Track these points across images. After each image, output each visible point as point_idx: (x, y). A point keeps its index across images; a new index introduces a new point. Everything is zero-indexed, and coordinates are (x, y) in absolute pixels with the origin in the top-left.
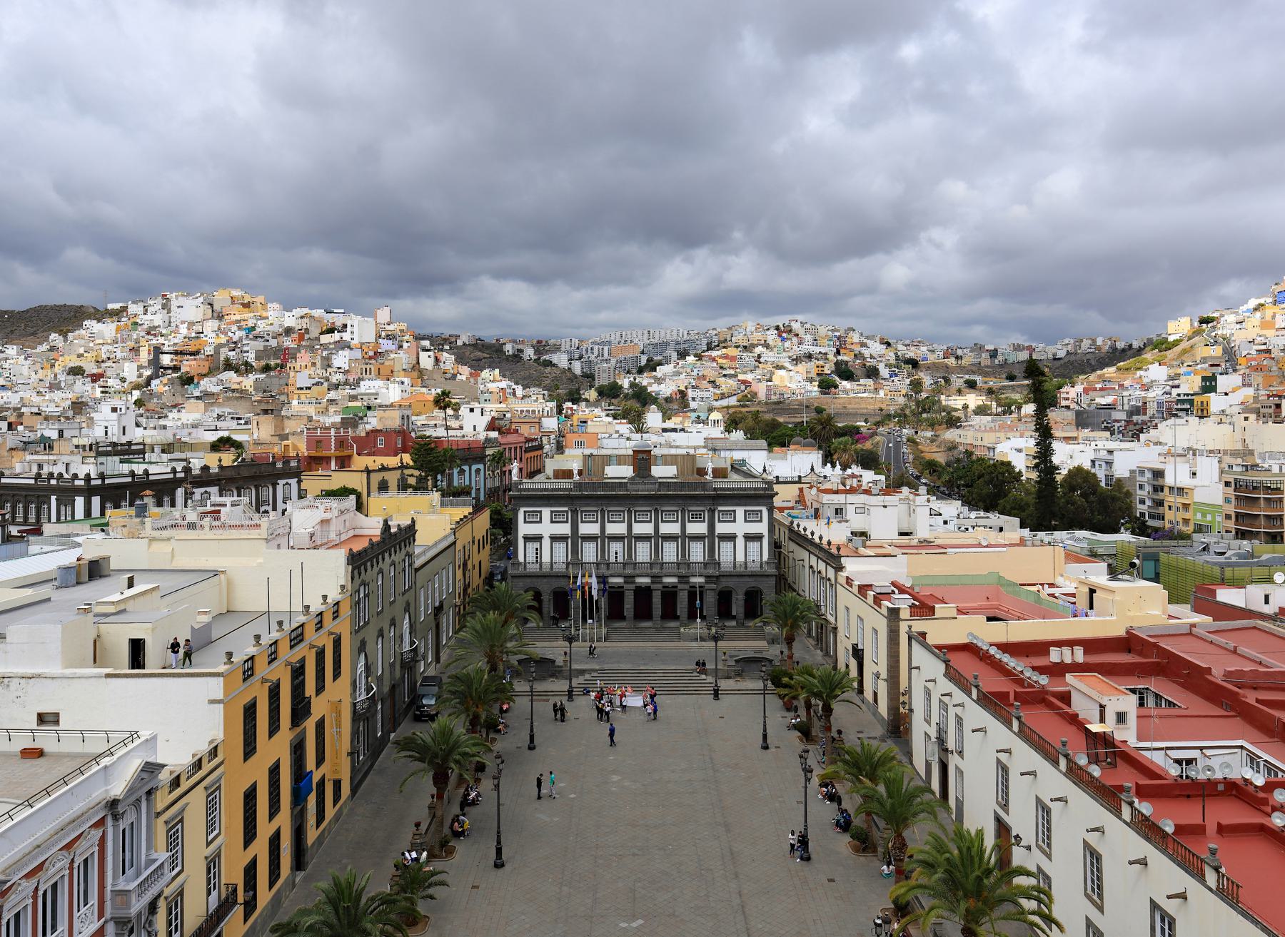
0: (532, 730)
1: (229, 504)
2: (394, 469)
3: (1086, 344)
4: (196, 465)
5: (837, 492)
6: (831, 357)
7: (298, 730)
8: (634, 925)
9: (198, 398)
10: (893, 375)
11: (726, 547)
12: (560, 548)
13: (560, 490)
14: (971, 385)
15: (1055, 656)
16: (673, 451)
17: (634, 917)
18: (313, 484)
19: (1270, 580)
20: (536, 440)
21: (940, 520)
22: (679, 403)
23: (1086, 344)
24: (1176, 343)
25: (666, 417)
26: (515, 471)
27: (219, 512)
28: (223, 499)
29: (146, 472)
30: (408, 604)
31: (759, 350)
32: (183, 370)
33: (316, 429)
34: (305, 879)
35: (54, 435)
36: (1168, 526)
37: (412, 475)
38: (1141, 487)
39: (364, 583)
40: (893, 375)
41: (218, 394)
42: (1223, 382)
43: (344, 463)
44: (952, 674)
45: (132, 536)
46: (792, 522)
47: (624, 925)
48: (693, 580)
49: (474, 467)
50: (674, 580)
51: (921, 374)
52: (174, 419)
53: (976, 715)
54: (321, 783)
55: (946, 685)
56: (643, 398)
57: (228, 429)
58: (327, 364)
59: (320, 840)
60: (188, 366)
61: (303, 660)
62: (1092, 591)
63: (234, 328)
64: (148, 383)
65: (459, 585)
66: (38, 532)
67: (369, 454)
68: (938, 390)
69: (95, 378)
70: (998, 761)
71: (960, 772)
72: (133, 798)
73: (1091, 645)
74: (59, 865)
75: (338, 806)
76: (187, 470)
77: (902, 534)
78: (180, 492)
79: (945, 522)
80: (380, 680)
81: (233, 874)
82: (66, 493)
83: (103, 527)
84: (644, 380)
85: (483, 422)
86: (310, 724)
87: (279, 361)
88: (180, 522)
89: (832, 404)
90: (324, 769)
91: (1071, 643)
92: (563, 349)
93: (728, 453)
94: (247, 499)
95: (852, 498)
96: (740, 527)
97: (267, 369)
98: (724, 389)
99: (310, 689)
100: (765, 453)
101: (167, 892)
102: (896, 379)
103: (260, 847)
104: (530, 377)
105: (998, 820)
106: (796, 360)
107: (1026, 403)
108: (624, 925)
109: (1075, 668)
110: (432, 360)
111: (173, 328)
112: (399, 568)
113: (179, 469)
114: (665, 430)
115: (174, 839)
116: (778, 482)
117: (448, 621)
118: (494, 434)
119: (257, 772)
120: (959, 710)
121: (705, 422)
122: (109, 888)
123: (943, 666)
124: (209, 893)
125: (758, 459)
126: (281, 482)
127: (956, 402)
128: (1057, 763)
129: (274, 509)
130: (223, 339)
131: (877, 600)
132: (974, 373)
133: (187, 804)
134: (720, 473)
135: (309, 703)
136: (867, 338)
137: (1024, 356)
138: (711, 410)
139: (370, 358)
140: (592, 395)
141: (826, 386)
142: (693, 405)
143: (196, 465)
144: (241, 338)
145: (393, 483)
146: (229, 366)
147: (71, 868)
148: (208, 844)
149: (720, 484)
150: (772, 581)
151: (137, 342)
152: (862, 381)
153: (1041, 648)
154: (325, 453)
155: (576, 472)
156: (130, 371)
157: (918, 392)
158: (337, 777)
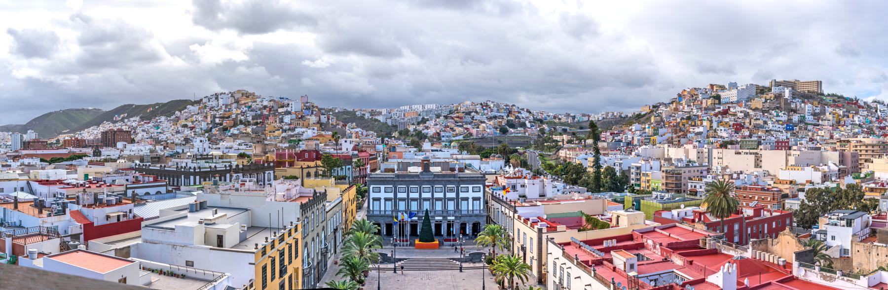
3: (610, 116)
4: (234, 164)
10: (532, 126)
11: (464, 203)
12: (389, 203)
14: (565, 131)
15: (605, 244)
16: (438, 160)
18: (280, 171)
19: (679, 207)
22: (437, 138)
23: (610, 116)
24: (645, 115)
31: (473, 114)
35: (181, 151)
39: (307, 217)
40: (532, 126)
42: (661, 131)
43: (291, 165)
44: (565, 254)
45: (212, 192)
50: (441, 218)
52: (223, 144)
53: (576, 271)
55: (563, 260)
56: (421, 136)
57: (243, 149)
58: (281, 121)
62: (618, 217)
65: (344, 219)
66: (179, 189)
68: (551, 133)
69: (192, 128)
73: (620, 239)
76: (231, 166)
78: (228, 175)
80: (313, 260)
82: (187, 174)
83: (202, 189)
84: (420, 128)
86: (286, 277)
89: (506, 139)
91: (611, 238)
95: (519, 181)
96: (470, 195)
97: (257, 124)
98: (457, 132)
99: (286, 262)
106: (490, 119)
117: (339, 235)
118: (356, 152)
120: (569, 270)
121: (449, 147)
125: (476, 163)
127: (558, 138)
130: (239, 112)
134: (461, 170)
137: (586, 119)
138: (451, 142)
140: (396, 134)
141: (504, 131)
142: (443, 139)
143: (234, 164)
145: (313, 174)
146: (241, 122)
149: (461, 175)
150: (485, 219)
153: (599, 242)
156: (204, 125)
157: (544, 133)
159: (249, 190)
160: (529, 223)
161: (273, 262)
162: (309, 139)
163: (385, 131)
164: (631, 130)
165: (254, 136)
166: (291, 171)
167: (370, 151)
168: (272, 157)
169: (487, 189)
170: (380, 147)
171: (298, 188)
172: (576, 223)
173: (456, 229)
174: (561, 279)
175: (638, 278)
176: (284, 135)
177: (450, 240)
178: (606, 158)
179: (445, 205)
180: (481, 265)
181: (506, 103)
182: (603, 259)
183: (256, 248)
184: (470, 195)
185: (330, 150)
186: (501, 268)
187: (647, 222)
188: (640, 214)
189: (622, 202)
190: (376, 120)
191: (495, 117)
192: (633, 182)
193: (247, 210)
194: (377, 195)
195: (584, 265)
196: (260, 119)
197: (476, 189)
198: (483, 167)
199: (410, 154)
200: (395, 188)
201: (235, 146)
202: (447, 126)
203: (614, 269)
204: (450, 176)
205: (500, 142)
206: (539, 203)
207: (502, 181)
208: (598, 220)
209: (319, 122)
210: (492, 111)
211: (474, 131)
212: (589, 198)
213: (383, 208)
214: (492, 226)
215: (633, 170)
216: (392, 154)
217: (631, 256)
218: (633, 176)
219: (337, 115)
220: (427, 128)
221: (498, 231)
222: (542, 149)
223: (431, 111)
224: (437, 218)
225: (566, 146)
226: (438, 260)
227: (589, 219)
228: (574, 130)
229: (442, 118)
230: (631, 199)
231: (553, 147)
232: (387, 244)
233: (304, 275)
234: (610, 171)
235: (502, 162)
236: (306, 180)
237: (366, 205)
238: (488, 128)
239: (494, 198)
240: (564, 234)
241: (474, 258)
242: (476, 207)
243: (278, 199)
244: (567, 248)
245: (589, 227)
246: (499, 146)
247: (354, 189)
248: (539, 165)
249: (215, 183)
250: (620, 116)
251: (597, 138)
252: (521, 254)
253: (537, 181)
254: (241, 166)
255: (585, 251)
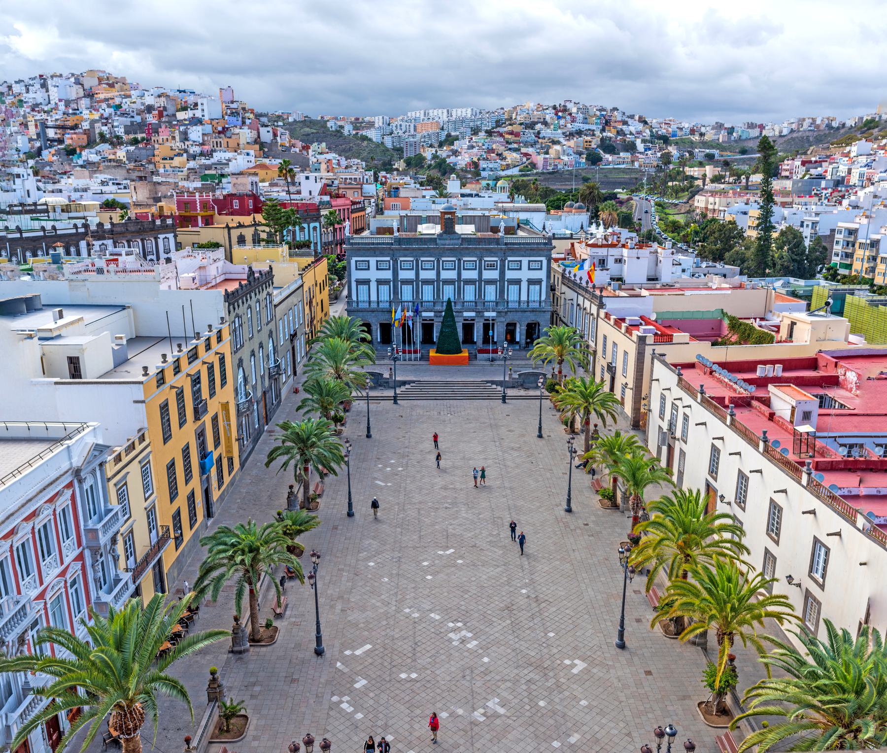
0: (368, 424)
1: (123, 253)
2: (249, 226)
3: (806, 125)
5: (602, 246)
6: (598, 133)
7: (199, 423)
8: (448, 552)
9: (82, 166)
10: (647, 149)
11: (513, 288)
12: (384, 289)
13: (383, 244)
14: (710, 158)
15: (760, 372)
16: (471, 213)
17: (447, 548)
18: (186, 235)
20: (360, 203)
21: (679, 268)
22: (474, 171)
23: (806, 125)
25: (463, 185)
26: (347, 229)
27: (117, 260)
28: (117, 250)
29: (54, 228)
30: (271, 332)
31: (539, 127)
32: (68, 142)
33: (182, 192)
34: (214, 523)
36: (853, 273)
37: (264, 231)
38: (837, 242)
39: (238, 316)
40: (647, 149)
41: (99, 163)
43: (208, 221)
46: (564, 270)
47: (441, 552)
48: (487, 314)
49: (312, 225)
50: (473, 314)
51: (670, 149)
52: (66, 183)
53: (699, 413)
54: (220, 459)
56: (444, 169)
58: (185, 137)
59: (221, 498)
60: (70, 139)
61: (199, 372)
62: (793, 324)
63: (104, 105)
64: (39, 152)
67: (226, 214)
68: (683, 163)
70: (713, 445)
71: (682, 453)
72: (90, 468)
73: (789, 365)
74: (46, 513)
75: (232, 475)
76: (86, 226)
77: (649, 280)
78: (83, 244)
79: (684, 271)
80: (254, 388)
81: (164, 519)
84: (443, 153)
85: (317, 187)
86: (207, 419)
87: (144, 135)
88: (90, 267)
90: (222, 449)
91: (773, 362)
92: (376, 125)
93: (515, 214)
94: (136, 250)
95: (612, 251)
97: (135, 142)
98: (509, 161)
99: (205, 394)
100: (544, 214)
101: (122, 530)
102: (649, 152)
103: (181, 502)
104: (350, 149)
105: (708, 485)
106: (570, 135)
107: (754, 173)
108: (441, 552)
109: (776, 380)
110: (271, 134)
111: (52, 105)
112: (263, 304)
113: (79, 225)
114: (463, 195)
115: (123, 496)
116: (555, 239)
117: (300, 344)
118: (326, 198)
119: (174, 450)
120: (687, 411)
121: (494, 189)
122: (82, 527)
123: (676, 377)
124: (150, 532)
125: (539, 220)
126: (161, 236)
127: (695, 172)
128: (758, 446)
129: (158, 259)
130: (96, 116)
131: (628, 331)
132: (713, 148)
133: (128, 473)
134: (509, 230)
135: (206, 403)
136: (628, 117)
137: (755, 133)
138: (497, 179)
139: (220, 132)
140: (400, 165)
141: (594, 159)
142: (483, 174)
144: (110, 115)
147: (55, 515)
148: (146, 500)
149: (510, 239)
150: (548, 316)
151: (25, 117)
152: (622, 154)
153: (750, 366)
154: (192, 213)
155: (395, 229)
158: (230, 455)
159: (124, 271)
160: (624, 325)
161: (180, 395)
162: (241, 174)
163: (382, 160)
164: (847, 155)
165: (131, 165)
166: (207, 234)
167: (352, 196)
168: (170, 207)
169: (554, 265)
170: (371, 189)
171: (220, 264)
172: (711, 331)
173: (498, 333)
174: (672, 425)
175: (815, 437)
176: (192, 164)
177: (487, 352)
178: (786, 212)
179: (480, 292)
180: (537, 393)
181: (600, 104)
182: (752, 398)
183: (146, 374)
184: (525, 274)
185: (280, 194)
186: (570, 400)
187: (852, 338)
188: (843, 322)
189: (808, 297)
190: (365, 138)
191: (579, 133)
192: (836, 260)
193: (123, 308)
194: (362, 275)
195: (716, 404)
196: (142, 133)
197: (533, 266)
198: (548, 224)
199: (421, 201)
200: (395, 262)
201: (95, 186)
202: (490, 151)
203: (772, 417)
204: (489, 241)
205: (586, 180)
206: (644, 293)
207: (582, 251)
208: (752, 328)
209: (257, 141)
210: (573, 120)
211: (539, 159)
212: (741, 287)
213: (374, 298)
214: (562, 329)
215: (838, 237)
216: (391, 201)
217: (808, 398)
218: (838, 248)
219: (292, 128)
220: (455, 153)
221: (569, 338)
222: (663, 194)
223: (463, 121)
224: (466, 314)
225: (710, 186)
226: (465, 384)
227: (736, 324)
228: (728, 155)
229: (482, 134)
230: (826, 293)
231: (683, 190)
232: (383, 358)
233: (239, 414)
234: (792, 237)
235: (584, 217)
236: (236, 248)
237: (345, 293)
238: (564, 154)
239: (566, 280)
240: (686, 348)
241: (526, 381)
242: (534, 297)
243: (184, 284)
244: (687, 374)
245: (734, 338)
246: (582, 187)
247: (324, 265)
248: (654, 222)
249: (56, 260)
250: (829, 126)
251: (772, 171)
252: (607, 377)
253: (645, 252)
254: (107, 226)
255: (720, 381)
